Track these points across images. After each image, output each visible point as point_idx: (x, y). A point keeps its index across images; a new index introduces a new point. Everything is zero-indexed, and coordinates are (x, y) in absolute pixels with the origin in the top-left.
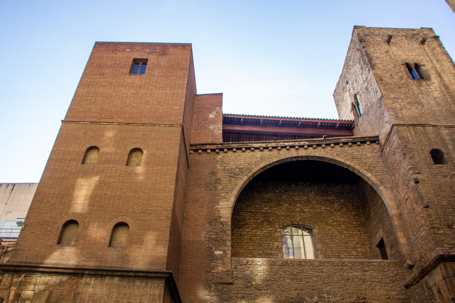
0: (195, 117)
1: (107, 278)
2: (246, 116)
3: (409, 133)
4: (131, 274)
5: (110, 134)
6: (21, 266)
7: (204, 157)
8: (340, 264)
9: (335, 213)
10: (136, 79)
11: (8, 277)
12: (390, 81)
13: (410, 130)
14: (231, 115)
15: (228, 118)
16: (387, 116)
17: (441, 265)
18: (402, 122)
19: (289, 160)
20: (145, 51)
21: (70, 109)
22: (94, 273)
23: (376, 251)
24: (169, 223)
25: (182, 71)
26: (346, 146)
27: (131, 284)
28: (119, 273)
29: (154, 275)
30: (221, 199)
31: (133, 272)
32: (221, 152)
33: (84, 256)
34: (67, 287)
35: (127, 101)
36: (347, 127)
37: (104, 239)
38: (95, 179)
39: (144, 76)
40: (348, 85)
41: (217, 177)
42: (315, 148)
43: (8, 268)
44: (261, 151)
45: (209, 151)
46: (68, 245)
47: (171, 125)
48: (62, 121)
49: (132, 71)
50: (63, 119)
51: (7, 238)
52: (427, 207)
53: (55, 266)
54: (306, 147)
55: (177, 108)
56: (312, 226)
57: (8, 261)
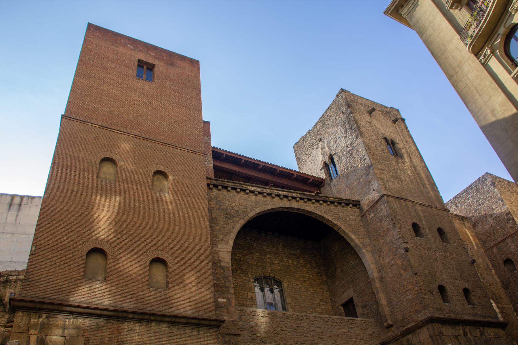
1: (153, 324)
2: (229, 152)
3: (396, 204)
4: (182, 320)
6: (44, 303)
8: (330, 320)
9: (301, 268)
12: (375, 152)
13: (396, 202)
16: (375, 185)
17: (430, 326)
18: (390, 194)
19: (281, 210)
20: (150, 54)
23: (339, 310)
25: (195, 91)
26: (332, 205)
27: (182, 332)
28: (169, 319)
29: (207, 323)
30: (219, 241)
31: (184, 318)
33: (121, 295)
36: (317, 184)
38: (117, 200)
40: (321, 143)
41: (213, 216)
42: (305, 202)
43: (25, 304)
44: (256, 195)
47: (194, 152)
52: (416, 274)
54: (298, 199)
56: (282, 280)
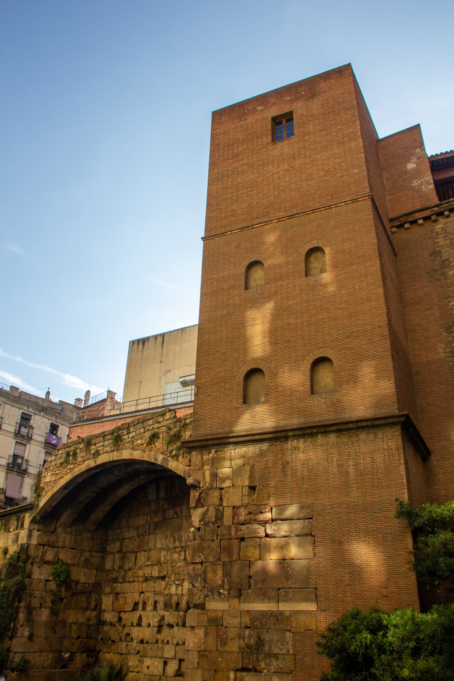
0: (385, 176)
1: (319, 436)
4: (351, 426)
5: (271, 238)
6: (207, 440)
7: (416, 233)
10: (285, 147)
14: (442, 154)
15: (438, 161)
21: (208, 219)
22: (301, 432)
24: (387, 344)
27: (354, 439)
28: (335, 428)
29: (383, 422)
31: (352, 422)
32: (440, 218)
33: (282, 413)
34: (270, 458)
35: (281, 184)
37: (303, 385)
38: (269, 306)
39: (294, 139)
41: (443, 259)
45: (421, 221)
46: (258, 402)
47: (353, 201)
48: (202, 238)
49: (276, 137)
50: (203, 236)
51: (175, 405)
53: (248, 433)
55: (356, 171)
57: (191, 435)
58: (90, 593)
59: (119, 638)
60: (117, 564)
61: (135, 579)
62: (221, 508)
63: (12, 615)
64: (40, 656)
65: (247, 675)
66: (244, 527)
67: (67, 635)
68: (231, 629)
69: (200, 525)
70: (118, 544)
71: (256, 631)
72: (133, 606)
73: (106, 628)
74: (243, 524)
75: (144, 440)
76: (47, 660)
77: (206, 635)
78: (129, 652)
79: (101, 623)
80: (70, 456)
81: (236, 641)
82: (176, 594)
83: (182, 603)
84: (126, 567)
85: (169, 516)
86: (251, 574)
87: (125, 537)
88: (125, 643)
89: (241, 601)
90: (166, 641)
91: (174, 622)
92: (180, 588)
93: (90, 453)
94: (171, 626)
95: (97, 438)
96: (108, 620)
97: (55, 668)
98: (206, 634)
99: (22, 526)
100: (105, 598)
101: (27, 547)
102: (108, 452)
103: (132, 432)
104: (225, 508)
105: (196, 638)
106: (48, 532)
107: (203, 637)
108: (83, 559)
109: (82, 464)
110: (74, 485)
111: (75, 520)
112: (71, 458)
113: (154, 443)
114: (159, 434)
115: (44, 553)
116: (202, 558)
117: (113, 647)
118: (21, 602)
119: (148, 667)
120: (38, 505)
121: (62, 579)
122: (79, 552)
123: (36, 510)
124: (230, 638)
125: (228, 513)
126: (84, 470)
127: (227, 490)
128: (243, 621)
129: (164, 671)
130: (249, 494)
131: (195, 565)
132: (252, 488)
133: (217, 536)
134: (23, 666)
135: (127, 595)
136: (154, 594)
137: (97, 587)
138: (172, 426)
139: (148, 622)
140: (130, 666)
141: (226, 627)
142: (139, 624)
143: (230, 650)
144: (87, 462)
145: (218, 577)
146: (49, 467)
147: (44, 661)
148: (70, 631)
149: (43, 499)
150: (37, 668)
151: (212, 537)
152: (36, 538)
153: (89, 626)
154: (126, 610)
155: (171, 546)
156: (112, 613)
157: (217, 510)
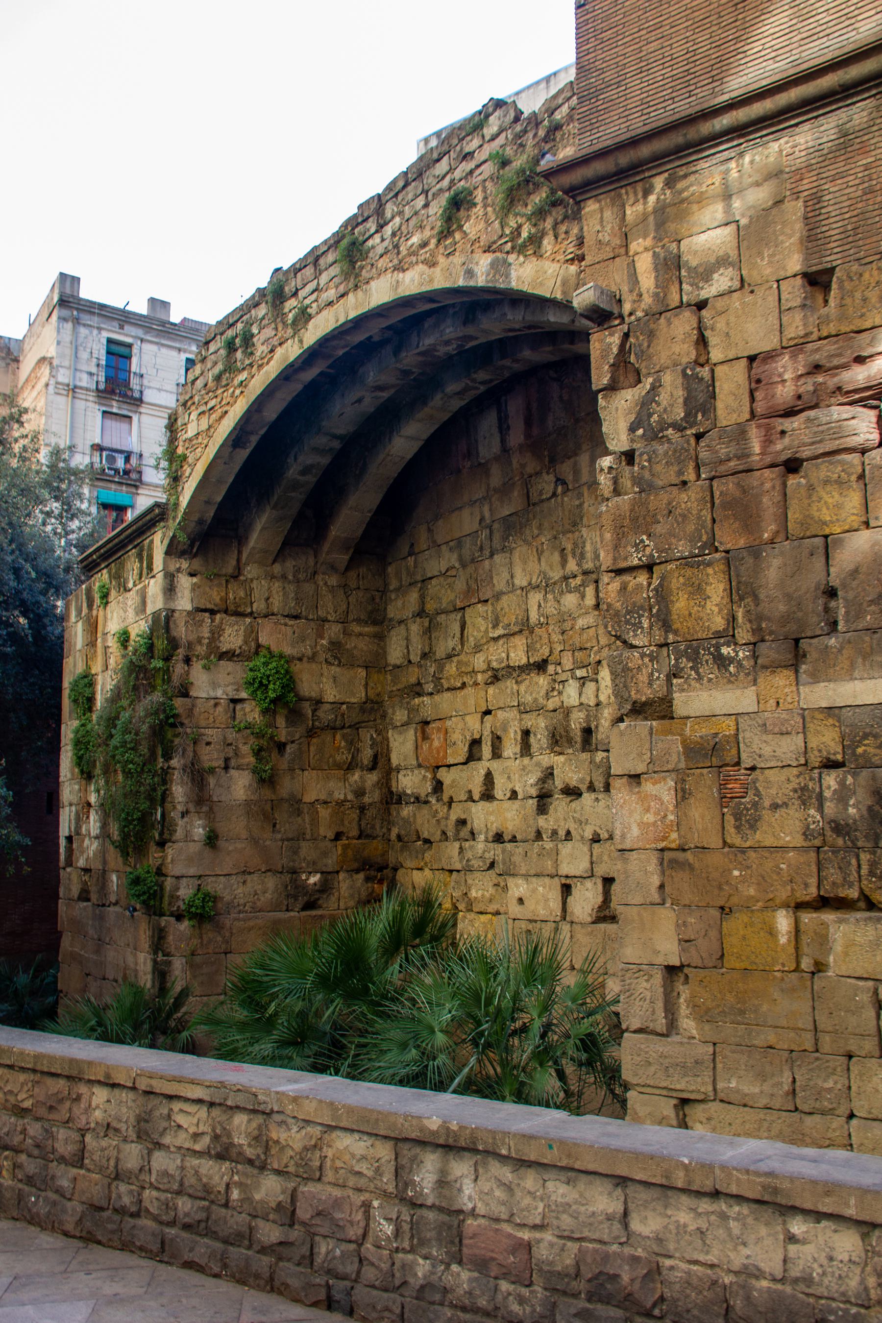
6: (634, 142)
11: (601, 210)
58: (356, 727)
59: (439, 833)
60: (417, 646)
61: (465, 680)
62: (705, 372)
63: (155, 790)
64: (244, 882)
65: (840, 921)
66: (794, 424)
67: (308, 831)
68: (772, 771)
69: (632, 441)
70: (413, 596)
71: (865, 773)
72: (466, 749)
73: (406, 811)
74: (790, 413)
75: (428, 228)
76: (264, 892)
77: (684, 798)
78: (468, 866)
79: (393, 799)
80: (236, 350)
81: (791, 812)
82: (581, 704)
83: (601, 729)
84: (440, 652)
85: (541, 493)
86: (835, 581)
87: (429, 575)
88: (457, 845)
89: (803, 677)
90: (562, 833)
91: (582, 780)
92: (590, 687)
93: (284, 323)
94: (572, 792)
95: (299, 275)
96: (409, 792)
97: (287, 910)
98: (683, 795)
99: (150, 568)
100: (396, 736)
101: (168, 618)
102: (330, 304)
103: (393, 217)
104: (719, 370)
105: (647, 810)
106: (217, 575)
107: (671, 808)
108: (324, 642)
109: (268, 363)
110: (262, 432)
111: (285, 544)
112: (239, 355)
113: (460, 227)
114: (470, 193)
115: (216, 634)
116: (648, 551)
117: (428, 856)
118: (171, 758)
119: (521, 901)
120: (177, 505)
121: (272, 695)
122: (312, 624)
123: (174, 518)
124: (767, 803)
125: (731, 384)
126: (273, 376)
127: (720, 304)
128: (813, 743)
129: (564, 909)
130: (808, 302)
131: (626, 578)
132: (817, 281)
133: (697, 468)
134: (203, 907)
135: (448, 723)
136: (521, 713)
137: (373, 710)
138: (509, 151)
139: (510, 786)
140: (476, 898)
141: (753, 769)
142: (488, 796)
143: (769, 841)
144: (279, 351)
145: (708, 605)
146: (191, 398)
147: (256, 894)
148: (315, 822)
149: (186, 486)
150: (239, 912)
151: (680, 473)
152: (187, 594)
153: (362, 809)
154: (450, 760)
155: (556, 575)
156: (416, 772)
157: (689, 380)
